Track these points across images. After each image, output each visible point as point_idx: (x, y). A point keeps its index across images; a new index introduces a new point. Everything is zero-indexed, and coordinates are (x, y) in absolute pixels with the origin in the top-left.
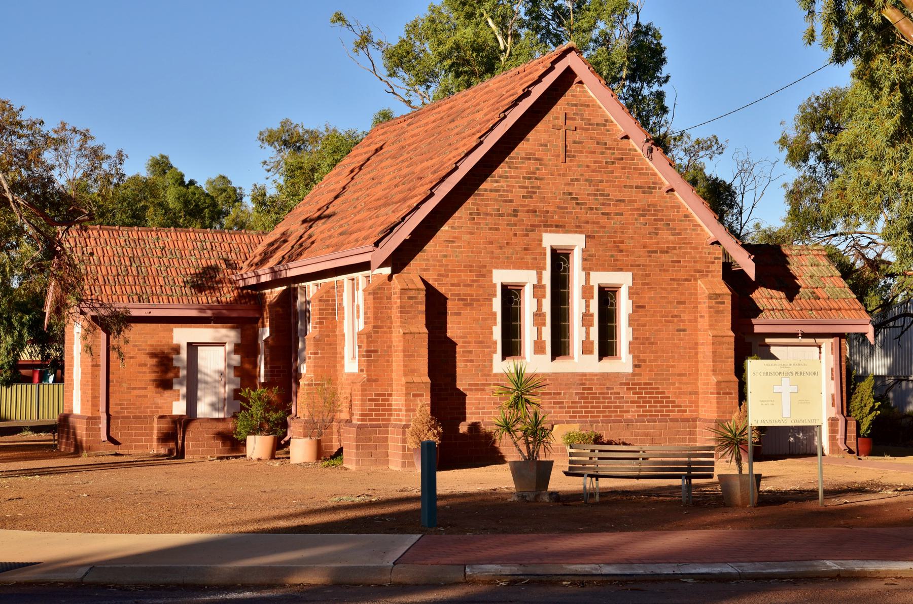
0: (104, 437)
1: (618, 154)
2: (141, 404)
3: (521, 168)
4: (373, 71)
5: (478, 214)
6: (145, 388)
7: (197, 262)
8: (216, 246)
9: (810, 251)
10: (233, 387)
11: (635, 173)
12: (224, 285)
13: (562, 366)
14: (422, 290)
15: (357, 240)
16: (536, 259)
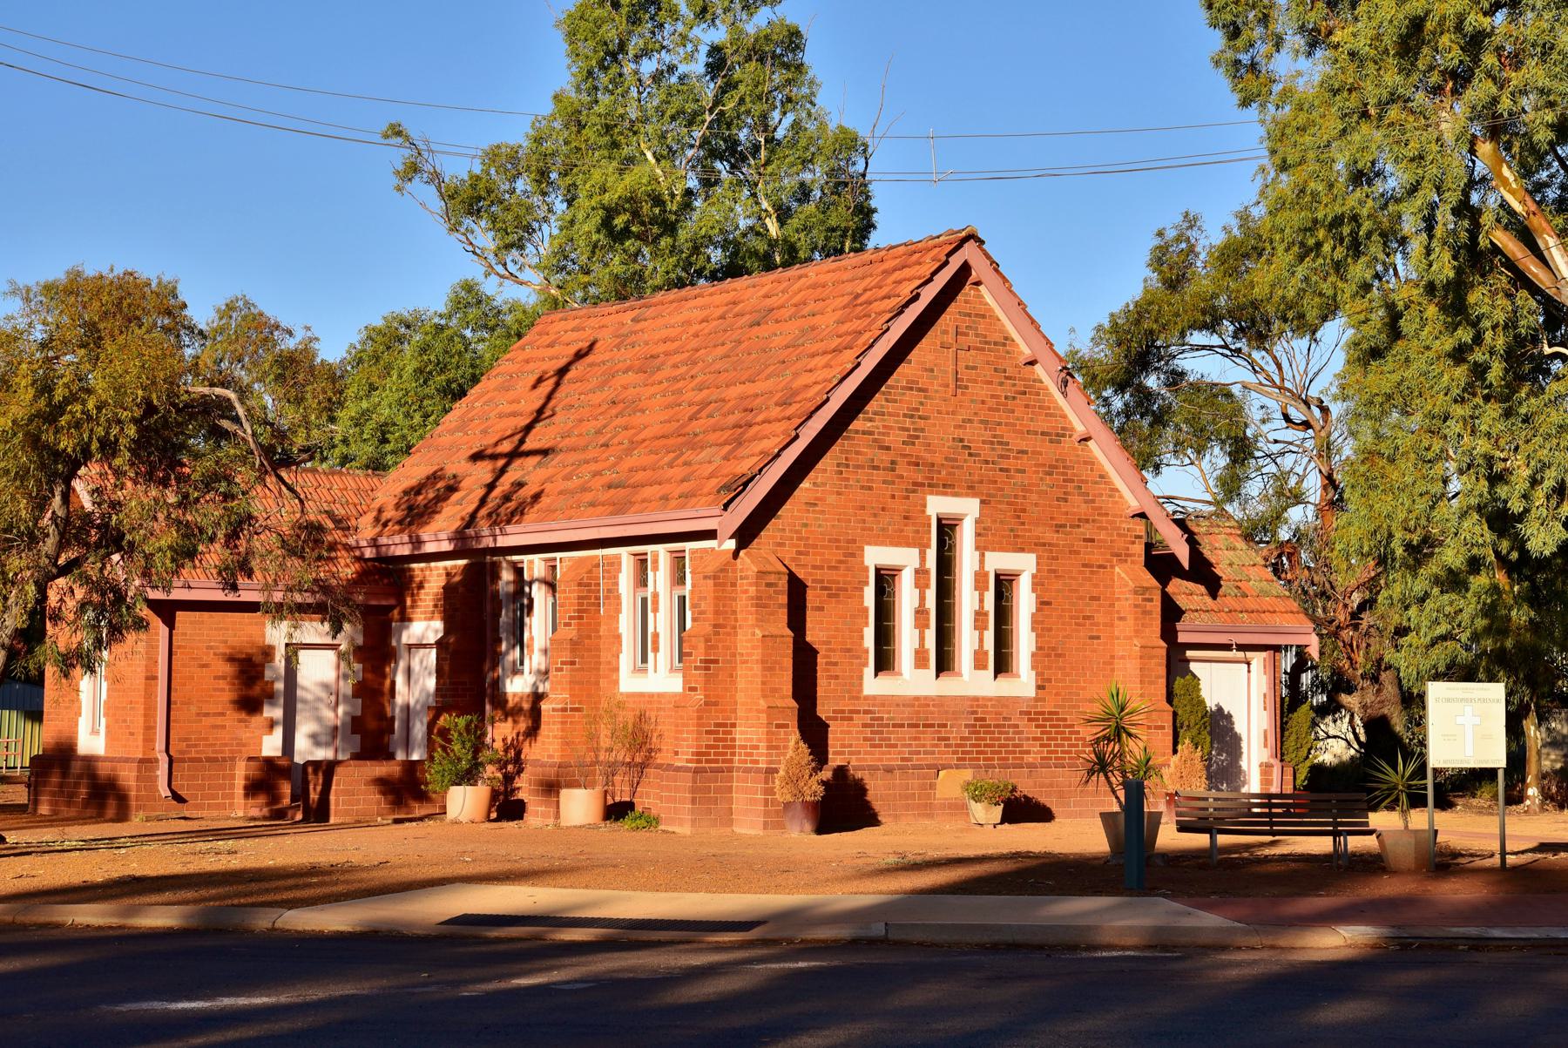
0: (164, 791)
3: (901, 401)
5: (847, 466)
6: (223, 714)
11: (1040, 414)
15: (665, 498)
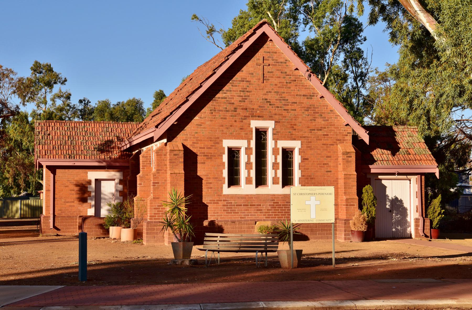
1: (293, 78)
2: (71, 210)
3: (238, 86)
4: (214, 42)
5: (215, 111)
6: (73, 202)
7: (102, 138)
8: (114, 130)
9: (409, 129)
10: (119, 201)
11: (302, 88)
12: (115, 149)
13: (262, 190)
14: (181, 150)
16: (247, 134)
